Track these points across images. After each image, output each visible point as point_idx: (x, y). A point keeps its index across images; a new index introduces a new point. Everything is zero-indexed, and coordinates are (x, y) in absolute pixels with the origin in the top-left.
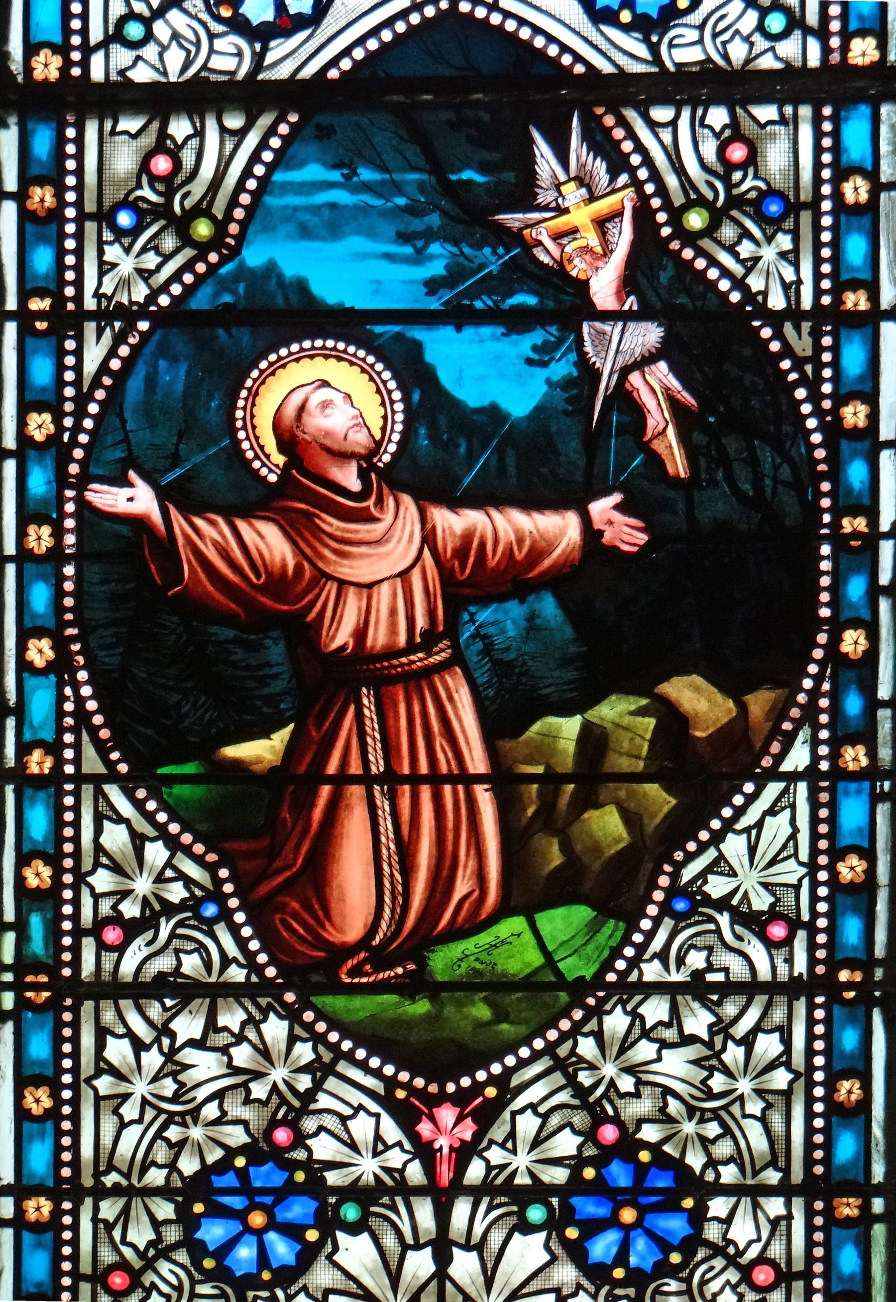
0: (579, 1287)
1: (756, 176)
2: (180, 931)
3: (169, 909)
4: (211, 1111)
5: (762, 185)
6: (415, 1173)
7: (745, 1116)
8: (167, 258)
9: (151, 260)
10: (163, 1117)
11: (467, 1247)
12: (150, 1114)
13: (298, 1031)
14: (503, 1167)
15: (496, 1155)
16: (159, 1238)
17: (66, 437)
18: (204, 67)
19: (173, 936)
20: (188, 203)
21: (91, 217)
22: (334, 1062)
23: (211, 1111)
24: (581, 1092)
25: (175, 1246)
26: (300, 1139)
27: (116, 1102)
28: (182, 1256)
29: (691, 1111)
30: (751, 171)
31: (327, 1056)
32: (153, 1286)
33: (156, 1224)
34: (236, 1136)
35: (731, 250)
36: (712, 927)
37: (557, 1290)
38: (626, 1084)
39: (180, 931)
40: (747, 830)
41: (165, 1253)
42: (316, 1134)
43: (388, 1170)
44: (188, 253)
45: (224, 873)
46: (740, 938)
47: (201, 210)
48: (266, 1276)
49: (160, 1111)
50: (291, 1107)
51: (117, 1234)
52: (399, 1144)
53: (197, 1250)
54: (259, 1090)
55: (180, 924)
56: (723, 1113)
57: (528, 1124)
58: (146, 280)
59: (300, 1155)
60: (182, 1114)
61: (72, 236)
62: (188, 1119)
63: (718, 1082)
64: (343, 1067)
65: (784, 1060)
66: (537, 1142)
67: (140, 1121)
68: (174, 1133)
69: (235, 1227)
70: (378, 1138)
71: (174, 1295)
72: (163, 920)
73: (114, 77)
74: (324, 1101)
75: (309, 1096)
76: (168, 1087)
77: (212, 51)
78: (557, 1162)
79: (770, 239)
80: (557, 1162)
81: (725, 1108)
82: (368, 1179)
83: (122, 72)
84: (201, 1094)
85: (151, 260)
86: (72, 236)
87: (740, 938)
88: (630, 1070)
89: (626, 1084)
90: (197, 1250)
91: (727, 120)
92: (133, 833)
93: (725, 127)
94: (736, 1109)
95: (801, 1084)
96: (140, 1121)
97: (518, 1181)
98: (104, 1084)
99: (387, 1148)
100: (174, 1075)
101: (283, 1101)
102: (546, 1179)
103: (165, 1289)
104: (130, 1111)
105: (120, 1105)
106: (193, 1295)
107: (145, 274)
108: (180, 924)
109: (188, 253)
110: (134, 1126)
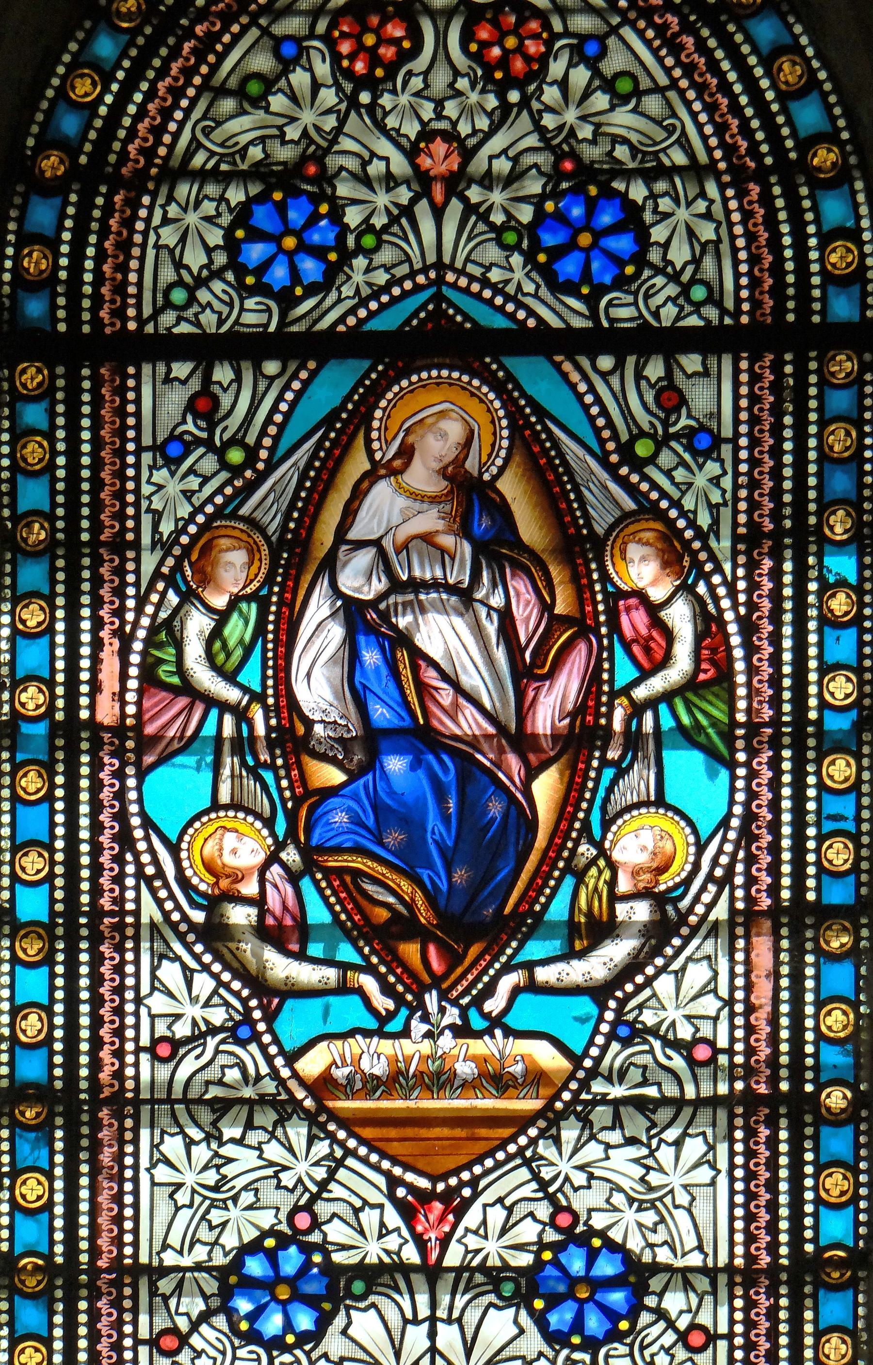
0: (541, 1354)
1: (689, 416)
2: (222, 1047)
3: (213, 1031)
4: (247, 1198)
5: (693, 423)
6: (410, 1254)
7: (676, 1207)
8: (206, 480)
9: (193, 482)
10: (208, 1202)
11: (449, 1321)
12: (198, 1199)
13: (315, 1130)
14: (477, 1251)
15: (473, 1242)
16: (211, 261)
17: (128, 628)
18: (236, 322)
19: (217, 1052)
20: (226, 437)
21: (147, 449)
22: (344, 1157)
23: (247, 1198)
24: (543, 1185)
25: (223, 269)
26: (316, 1224)
27: (170, 1020)
28: (230, 276)
29: (631, 1200)
30: (684, 411)
31: (339, 1153)
32: (209, 304)
33: (209, 251)
34: (266, 1219)
35: (668, 474)
36: (646, 1047)
37: (523, 1358)
38: (579, 1179)
39: (222, 1047)
40: (676, 972)
41: (218, 274)
42: (329, 1221)
43: (388, 1252)
44: (224, 475)
45: (253, 1003)
46: (670, 1058)
47: (235, 441)
48: (290, 1339)
49: (205, 1198)
50: (318, 146)
51: (173, 1303)
52: (398, 1229)
53: (241, 270)
54: (293, 133)
55: (223, 1042)
56: (658, 1204)
57: (497, 1216)
58: (189, 500)
59: (315, 1237)
60: (224, 1201)
61: (129, 1297)
62: (230, 1203)
63: (654, 1178)
64: (350, 1162)
65: (709, 988)
66: (504, 1231)
67: (191, 1206)
68: (216, 1216)
69: (271, 248)
70: (382, 1224)
71: (220, 1358)
72: (209, 1038)
73: (162, 331)
74: (336, 1190)
75: (323, 1185)
76: (211, 1177)
77: (242, 309)
78: (520, 1247)
79: (701, 467)
80: (520, 1247)
81: (661, 1199)
82: (372, 1259)
83: (169, 329)
84: (239, 1183)
85: (193, 482)
86: (129, 1297)
87: (670, 1058)
88: (581, 1168)
89: (579, 1179)
90: (241, 270)
91: (662, 374)
92: (184, 967)
93: (660, 379)
94: (668, 1200)
95: (725, 1012)
96: (191, 1206)
97: (489, 1263)
98: (162, 1173)
99: (389, 1233)
100: (218, 1167)
101: (312, 141)
102: (513, 1263)
103: (212, 1353)
104: (182, 1197)
105: (173, 1022)
106: (234, 1358)
107: (188, 495)
108: (223, 1042)
109: (224, 475)
110: (185, 1210)
